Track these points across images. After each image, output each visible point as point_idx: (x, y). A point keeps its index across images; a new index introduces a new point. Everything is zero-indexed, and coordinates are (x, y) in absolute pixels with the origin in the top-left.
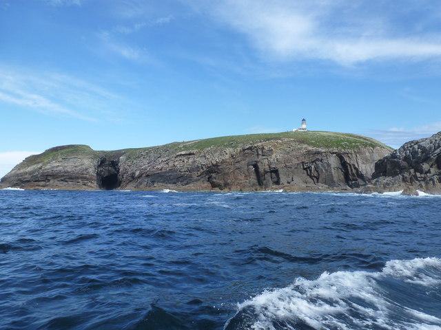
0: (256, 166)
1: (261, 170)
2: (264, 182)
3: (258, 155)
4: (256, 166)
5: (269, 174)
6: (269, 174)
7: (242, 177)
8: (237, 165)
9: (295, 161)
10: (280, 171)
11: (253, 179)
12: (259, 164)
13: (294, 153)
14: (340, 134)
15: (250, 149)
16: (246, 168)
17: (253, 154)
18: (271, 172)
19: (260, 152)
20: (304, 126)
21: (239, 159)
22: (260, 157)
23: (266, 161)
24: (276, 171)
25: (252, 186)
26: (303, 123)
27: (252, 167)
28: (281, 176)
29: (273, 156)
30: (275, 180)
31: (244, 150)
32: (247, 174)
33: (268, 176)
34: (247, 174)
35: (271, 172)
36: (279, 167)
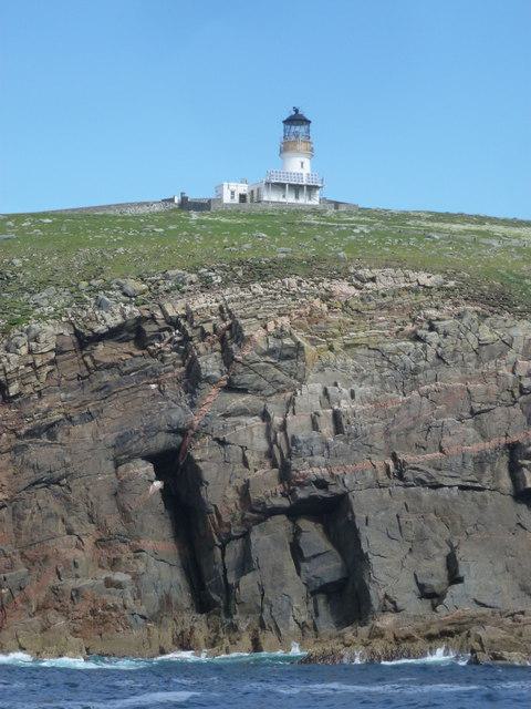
0: (175, 467)
1: (220, 492)
2: (247, 585)
3: (193, 380)
4: (175, 467)
5: (280, 525)
6: (280, 525)
7: (76, 551)
8: (42, 454)
9: (464, 440)
10: (365, 504)
11: (157, 563)
12: (202, 452)
13: (453, 378)
14: (109, 207)
15: (133, 332)
16: (105, 475)
17: (155, 375)
18: (295, 512)
19: (210, 364)
20: (299, 167)
21: (52, 405)
22: (211, 397)
23: (251, 433)
24: (331, 511)
25: (155, 619)
26: (286, 147)
27: (144, 469)
28: (372, 540)
29: (309, 394)
30: (328, 568)
31: (85, 341)
32: (114, 523)
33: (270, 541)
34: (114, 523)
35: (295, 512)
36: (358, 476)
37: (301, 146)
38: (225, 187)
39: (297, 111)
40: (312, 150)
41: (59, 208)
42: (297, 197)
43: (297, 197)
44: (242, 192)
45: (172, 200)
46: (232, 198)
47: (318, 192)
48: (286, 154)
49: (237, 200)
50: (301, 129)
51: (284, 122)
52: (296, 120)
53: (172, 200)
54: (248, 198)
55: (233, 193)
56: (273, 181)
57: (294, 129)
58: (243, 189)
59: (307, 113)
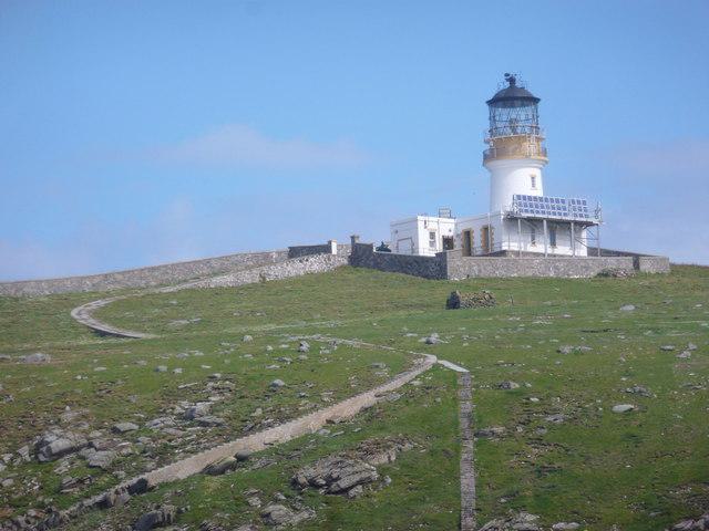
1: (374, 370)
26: (498, 150)
37: (530, 147)
38: (421, 225)
39: (512, 81)
40: (544, 153)
41: (62, 274)
42: (553, 244)
43: (553, 244)
44: (447, 234)
45: (326, 249)
46: (432, 244)
47: (584, 234)
48: (498, 164)
49: (439, 247)
50: (521, 113)
51: (493, 103)
52: (511, 97)
53: (326, 249)
54: (458, 244)
55: (432, 235)
56: (525, 215)
57: (504, 114)
58: (447, 227)
59: (530, 84)
